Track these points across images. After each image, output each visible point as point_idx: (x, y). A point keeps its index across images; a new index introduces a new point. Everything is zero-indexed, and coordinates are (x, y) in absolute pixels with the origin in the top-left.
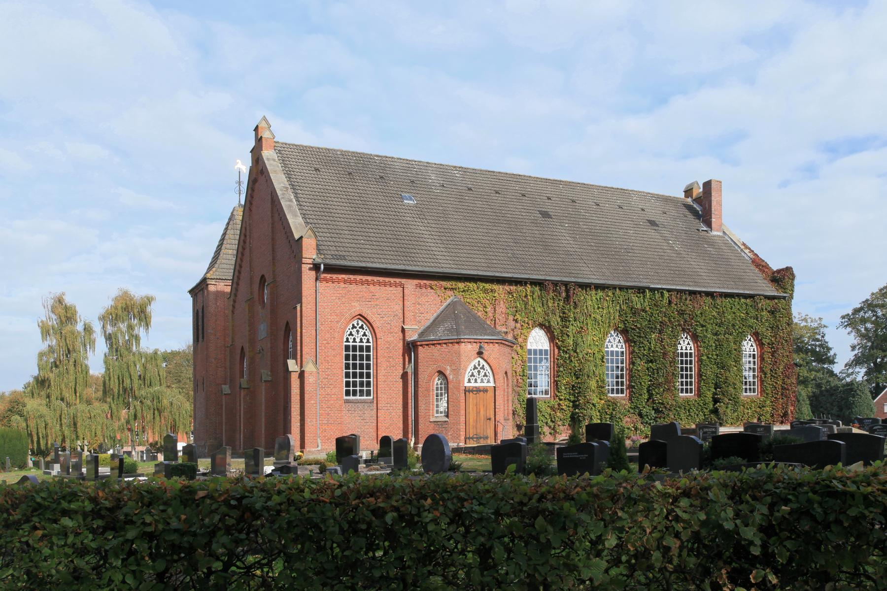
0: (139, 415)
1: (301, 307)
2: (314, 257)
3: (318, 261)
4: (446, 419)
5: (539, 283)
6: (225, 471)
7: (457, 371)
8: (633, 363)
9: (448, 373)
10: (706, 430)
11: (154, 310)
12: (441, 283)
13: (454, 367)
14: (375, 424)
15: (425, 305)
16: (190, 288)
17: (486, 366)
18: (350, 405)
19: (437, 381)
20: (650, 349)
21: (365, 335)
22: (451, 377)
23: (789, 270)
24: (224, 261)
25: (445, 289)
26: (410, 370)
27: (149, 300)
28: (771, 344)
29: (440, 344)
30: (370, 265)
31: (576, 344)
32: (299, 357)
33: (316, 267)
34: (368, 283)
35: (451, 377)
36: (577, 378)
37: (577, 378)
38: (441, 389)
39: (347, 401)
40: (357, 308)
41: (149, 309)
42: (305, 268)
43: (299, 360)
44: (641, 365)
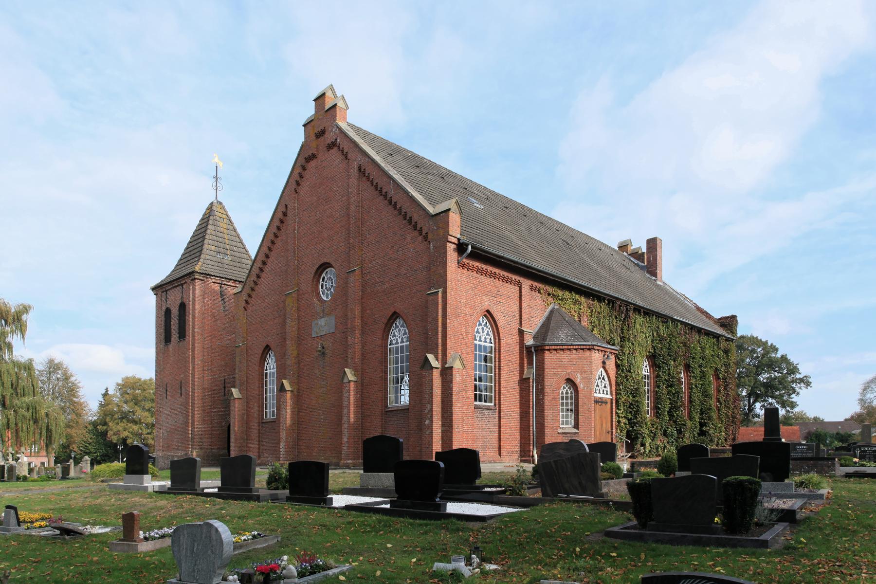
0: (12, 425)
1: (445, 293)
2: (459, 236)
3: (464, 239)
4: (576, 431)
5: (612, 301)
6: (251, 490)
7: (588, 380)
8: (658, 387)
9: (578, 381)
10: (863, 449)
11: (29, 319)
12: (547, 287)
13: (584, 375)
14: (497, 434)
15: (537, 307)
16: (154, 283)
17: (606, 378)
18: (479, 411)
19: (565, 390)
20: (669, 375)
21: (488, 334)
22: (581, 386)
23: (734, 317)
24: (208, 257)
25: (549, 294)
26: (531, 373)
27: (26, 309)
28: (725, 379)
29: (570, 349)
30: (508, 255)
31: (630, 364)
32: (440, 352)
33: (461, 248)
34: (493, 276)
35: (582, 386)
36: (634, 397)
37: (634, 397)
38: (571, 399)
39: (476, 407)
40: (486, 303)
41: (24, 317)
42: (450, 248)
43: (440, 357)
44: (664, 389)
